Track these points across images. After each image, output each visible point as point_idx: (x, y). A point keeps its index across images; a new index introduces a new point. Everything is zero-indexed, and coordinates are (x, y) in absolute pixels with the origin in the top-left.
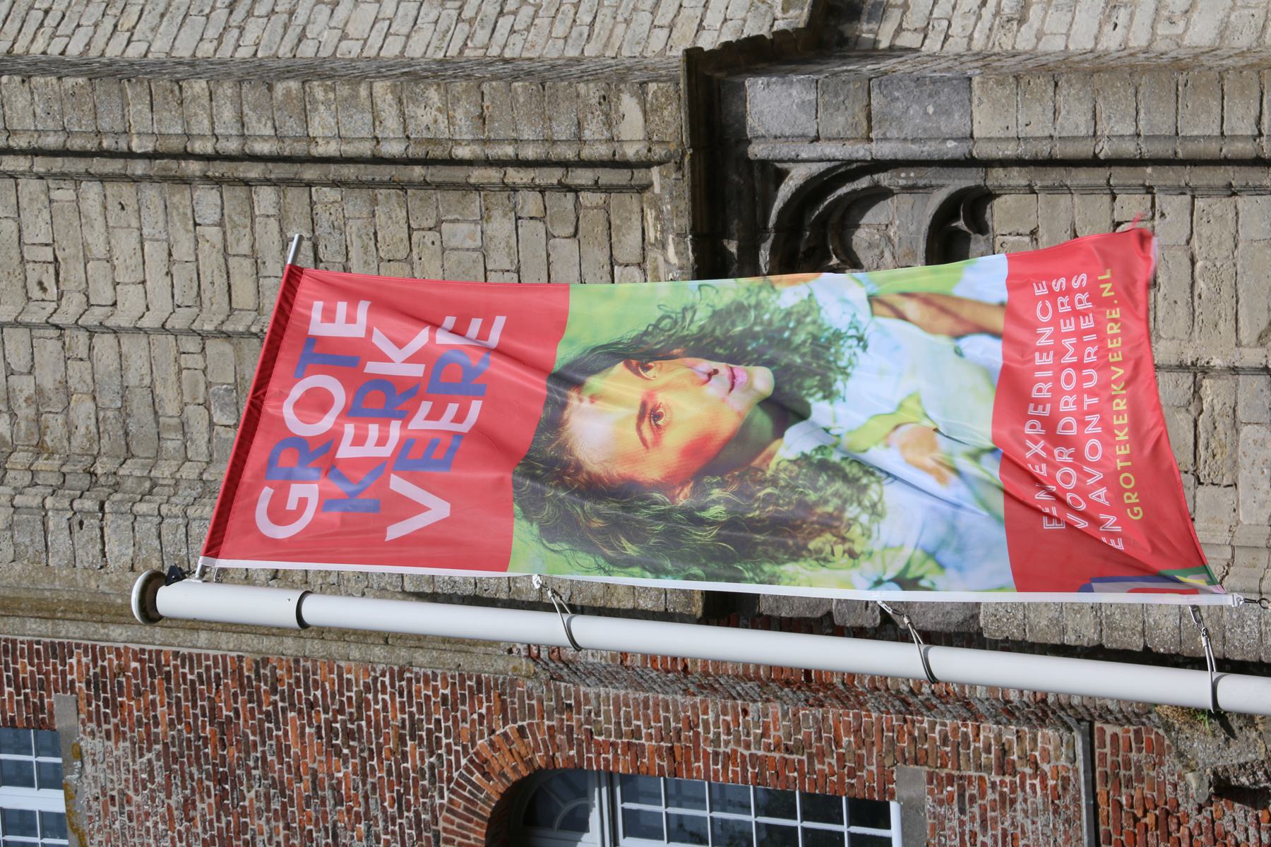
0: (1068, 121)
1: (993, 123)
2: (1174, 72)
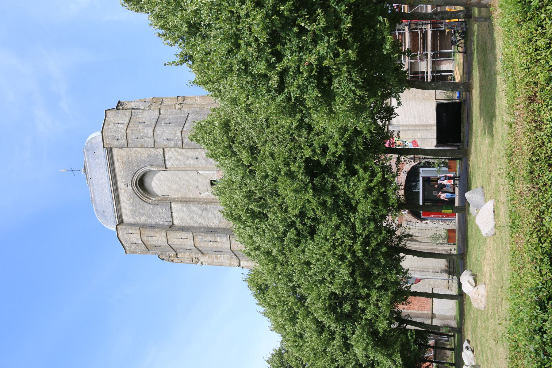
0: (404, 128)
1: (401, 128)
2: (408, 126)
